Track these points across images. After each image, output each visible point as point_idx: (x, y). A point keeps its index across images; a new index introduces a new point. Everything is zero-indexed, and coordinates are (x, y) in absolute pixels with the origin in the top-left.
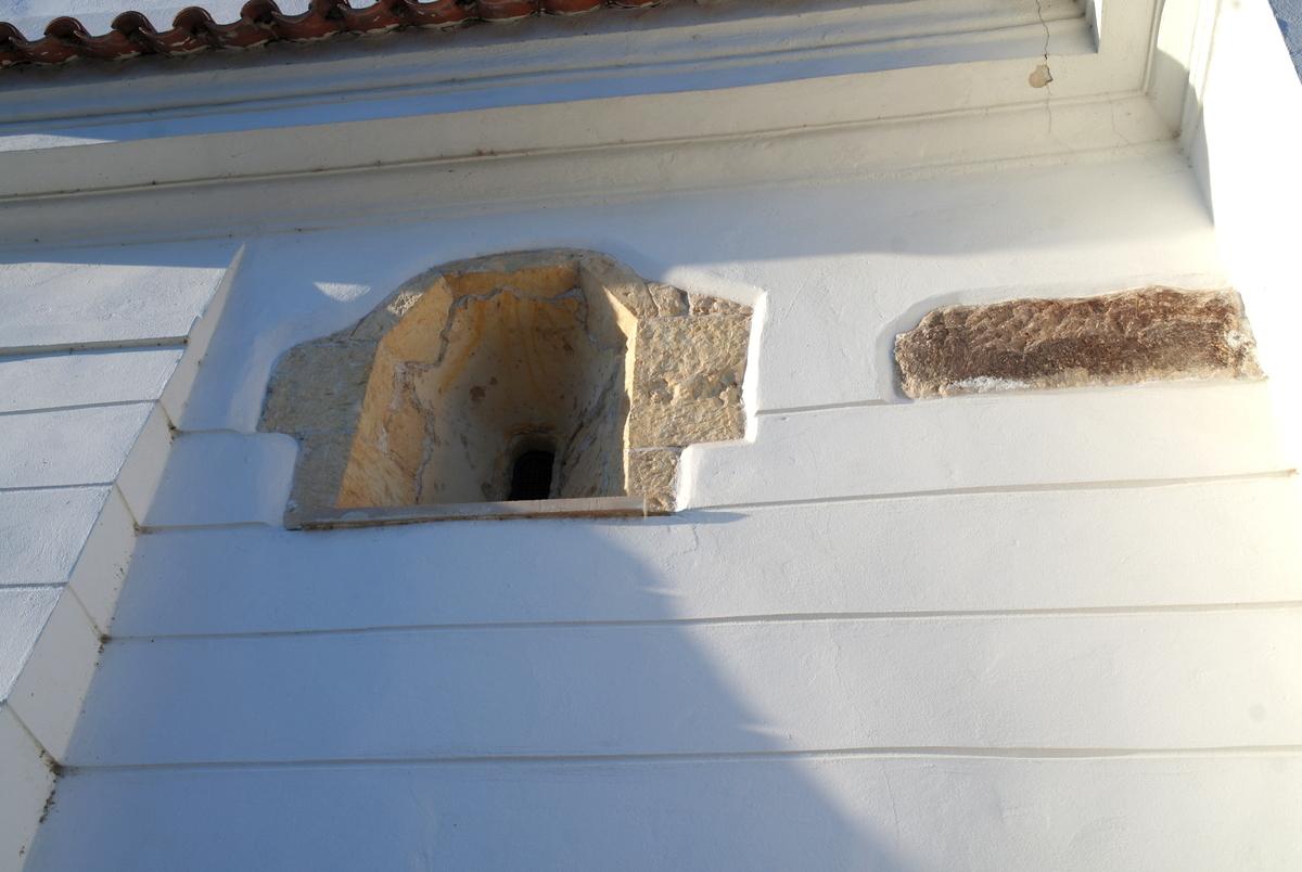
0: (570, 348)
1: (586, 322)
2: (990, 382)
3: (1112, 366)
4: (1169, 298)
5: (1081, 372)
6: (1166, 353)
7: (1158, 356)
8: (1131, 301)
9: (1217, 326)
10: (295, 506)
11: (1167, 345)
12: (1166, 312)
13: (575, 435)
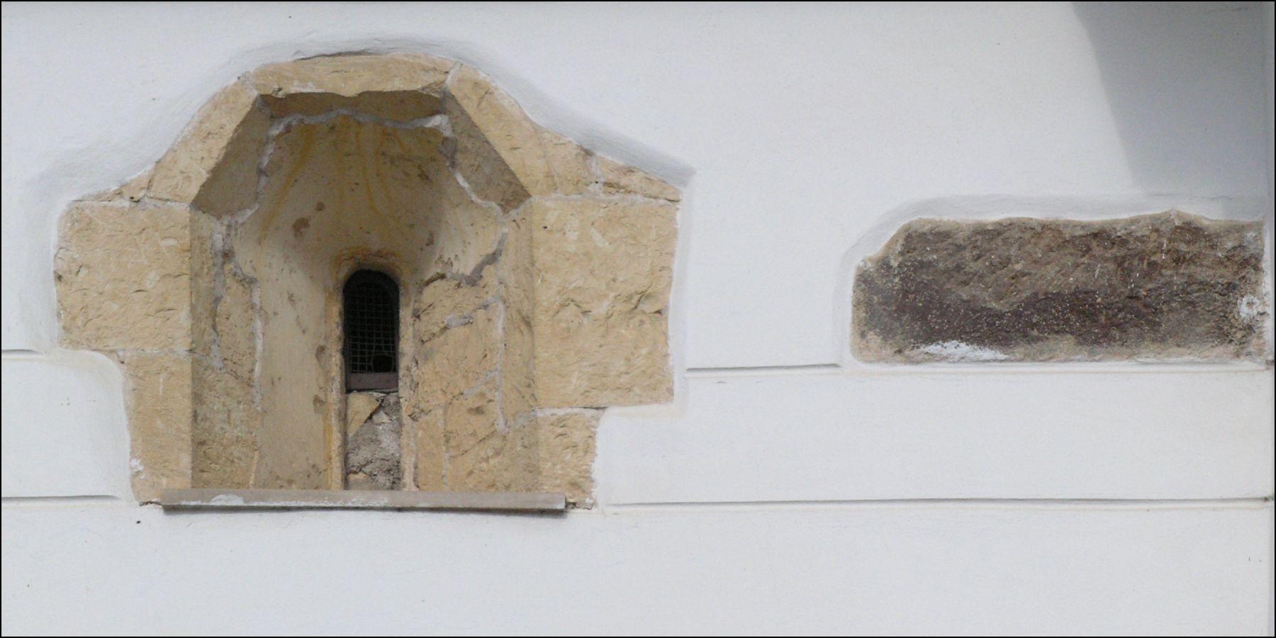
0: (427, 178)
1: (453, 157)
2: (964, 348)
3: (1105, 335)
4: (1188, 236)
5: (1067, 342)
6: (1169, 320)
7: (1159, 324)
8: (1141, 239)
9: (1231, 287)
10: (141, 468)
11: (1171, 310)
12: (1179, 260)
13: (432, 281)
